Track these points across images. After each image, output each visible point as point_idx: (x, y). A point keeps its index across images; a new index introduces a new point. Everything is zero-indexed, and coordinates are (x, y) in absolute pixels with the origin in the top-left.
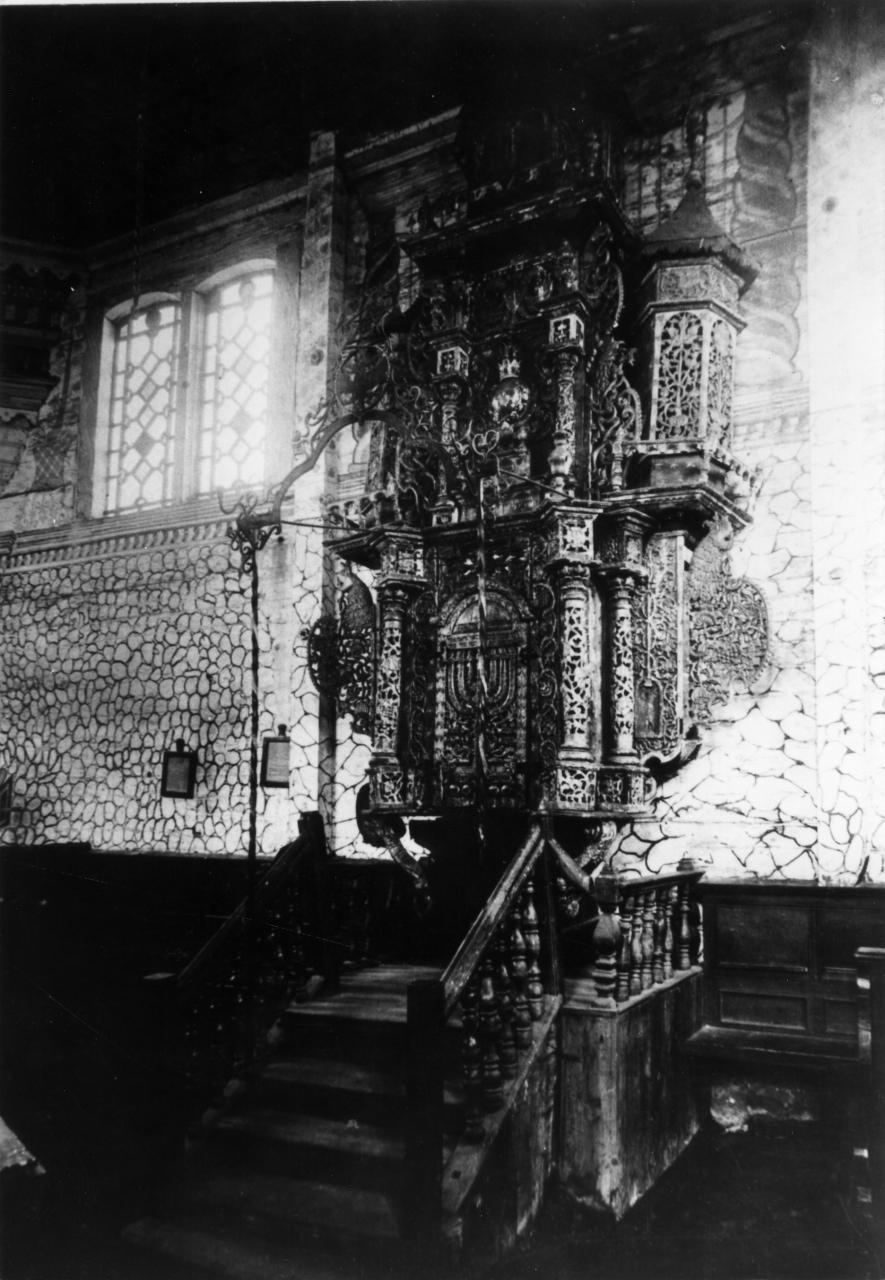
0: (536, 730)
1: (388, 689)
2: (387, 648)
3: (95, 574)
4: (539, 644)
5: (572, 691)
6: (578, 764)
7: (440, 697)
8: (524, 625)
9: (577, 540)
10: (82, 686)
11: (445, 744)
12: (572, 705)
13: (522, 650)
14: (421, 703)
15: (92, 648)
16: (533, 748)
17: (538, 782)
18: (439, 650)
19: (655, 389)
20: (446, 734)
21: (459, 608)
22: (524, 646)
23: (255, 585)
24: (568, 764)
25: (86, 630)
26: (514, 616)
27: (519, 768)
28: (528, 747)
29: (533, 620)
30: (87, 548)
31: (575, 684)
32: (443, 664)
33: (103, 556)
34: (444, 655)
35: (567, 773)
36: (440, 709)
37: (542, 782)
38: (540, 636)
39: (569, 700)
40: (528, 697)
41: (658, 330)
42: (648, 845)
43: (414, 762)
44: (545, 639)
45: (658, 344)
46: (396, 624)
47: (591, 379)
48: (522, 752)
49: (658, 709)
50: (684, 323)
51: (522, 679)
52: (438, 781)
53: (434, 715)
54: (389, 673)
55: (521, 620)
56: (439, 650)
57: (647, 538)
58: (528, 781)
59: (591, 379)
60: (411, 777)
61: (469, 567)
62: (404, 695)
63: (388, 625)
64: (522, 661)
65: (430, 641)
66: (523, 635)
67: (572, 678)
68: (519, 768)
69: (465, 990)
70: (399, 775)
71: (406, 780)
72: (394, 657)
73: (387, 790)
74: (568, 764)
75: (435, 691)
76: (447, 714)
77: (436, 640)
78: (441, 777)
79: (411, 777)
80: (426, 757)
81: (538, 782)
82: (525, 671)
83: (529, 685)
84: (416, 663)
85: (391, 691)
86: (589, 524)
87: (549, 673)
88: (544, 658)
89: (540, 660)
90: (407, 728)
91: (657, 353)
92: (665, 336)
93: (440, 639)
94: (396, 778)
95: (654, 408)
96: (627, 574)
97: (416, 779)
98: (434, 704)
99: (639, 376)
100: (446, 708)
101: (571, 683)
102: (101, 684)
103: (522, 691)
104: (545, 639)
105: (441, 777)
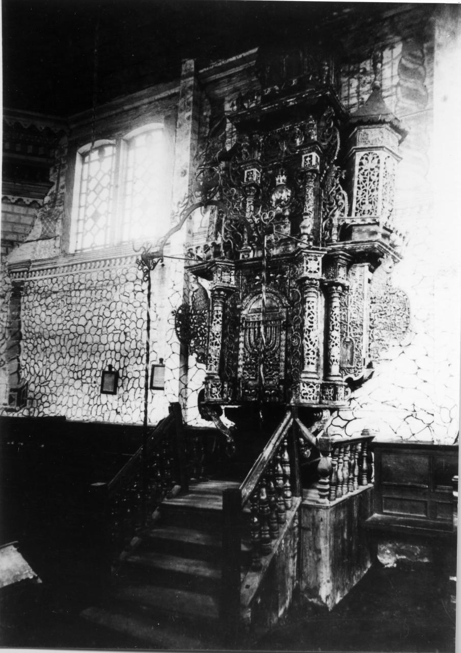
0: (290, 363)
1: (215, 341)
2: (215, 320)
3: (70, 281)
8: (285, 310)
9: (312, 268)
10: (62, 337)
11: (243, 369)
12: (308, 350)
14: (231, 348)
15: (68, 318)
16: (288, 372)
18: (241, 322)
19: (355, 190)
21: (252, 301)
22: (285, 320)
24: (306, 380)
25: (65, 309)
26: (280, 305)
27: (281, 382)
28: (285, 371)
30: (66, 268)
31: (310, 340)
32: (243, 329)
33: (74, 272)
34: (244, 324)
35: (305, 385)
36: (241, 352)
37: (292, 389)
38: (293, 316)
40: (286, 346)
41: (357, 161)
43: (227, 378)
45: (357, 168)
46: (220, 308)
47: (323, 186)
48: (282, 374)
49: (352, 353)
50: (370, 157)
51: (283, 337)
52: (240, 388)
53: (238, 355)
54: (215, 333)
55: (283, 307)
56: (241, 322)
57: (349, 266)
59: (323, 186)
60: (226, 386)
62: (223, 344)
64: (283, 328)
65: (237, 317)
66: (284, 315)
67: (309, 336)
68: (281, 382)
69: (252, 494)
70: (220, 384)
71: (223, 387)
73: (213, 392)
74: (306, 380)
75: (239, 342)
76: (245, 354)
77: (240, 317)
78: (241, 386)
79: (226, 386)
80: (233, 375)
81: (290, 389)
83: (286, 340)
84: (230, 328)
85: (216, 342)
86: (320, 259)
87: (297, 334)
88: (294, 327)
89: (293, 327)
90: (224, 361)
91: (357, 173)
92: (361, 164)
93: (242, 316)
95: (355, 201)
96: (338, 284)
97: (228, 387)
98: (238, 349)
99: (347, 184)
100: (244, 351)
101: (308, 339)
102: (72, 336)
103: (283, 343)
105: (241, 386)
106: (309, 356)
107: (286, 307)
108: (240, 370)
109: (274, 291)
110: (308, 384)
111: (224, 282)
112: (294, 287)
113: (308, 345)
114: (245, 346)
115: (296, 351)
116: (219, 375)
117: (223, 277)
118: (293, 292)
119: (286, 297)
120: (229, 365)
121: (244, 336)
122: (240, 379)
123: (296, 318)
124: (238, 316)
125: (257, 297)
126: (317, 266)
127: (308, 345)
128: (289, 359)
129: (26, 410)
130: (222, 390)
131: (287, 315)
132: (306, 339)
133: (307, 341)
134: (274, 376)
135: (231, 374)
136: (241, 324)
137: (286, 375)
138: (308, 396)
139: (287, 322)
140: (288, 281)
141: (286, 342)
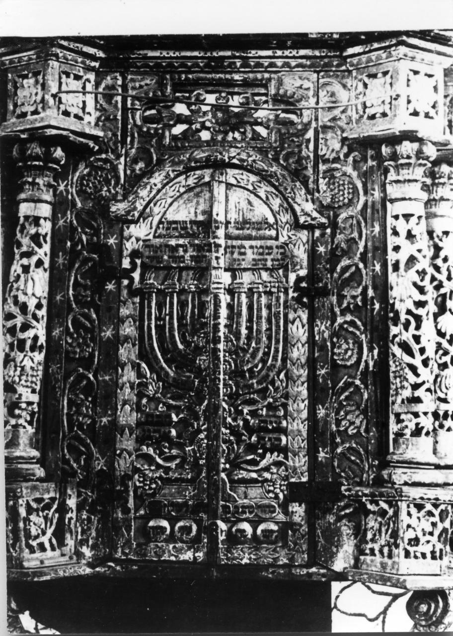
0: (326, 423)
1: (31, 333)
2: (28, 254)
4: (332, 270)
5: (417, 361)
6: (431, 493)
7: (126, 353)
8: (304, 235)
11: (140, 441)
12: (416, 387)
13: (299, 280)
14: (87, 363)
16: (322, 455)
17: (331, 519)
18: (126, 263)
20: (139, 424)
21: (171, 191)
22: (303, 273)
23: (248, 190)
24: (415, 493)
26: (285, 218)
27: (295, 493)
28: (312, 452)
29: (322, 226)
31: (422, 351)
32: (133, 293)
34: (136, 275)
35: (413, 510)
36: (129, 375)
37: (339, 519)
38: (334, 257)
39: (412, 379)
40: (312, 364)
42: (390, 598)
43: (74, 474)
44: (345, 262)
46: (45, 210)
48: (300, 462)
51: (299, 332)
52: (126, 511)
53: (116, 385)
54: (32, 303)
55: (297, 226)
56: (126, 263)
58: (311, 517)
60: (72, 503)
61: (180, 119)
62: (52, 349)
63: (25, 209)
64: (298, 300)
65: (108, 248)
66: (301, 254)
67: (417, 339)
68: (295, 493)
70: (53, 500)
71: (63, 509)
72: (40, 270)
73: (34, 531)
74: (415, 493)
75: (118, 341)
76: (143, 385)
77: (120, 245)
78: (131, 504)
79: (72, 503)
80: (100, 465)
81: (331, 519)
82: (305, 317)
83: (311, 341)
84: (76, 284)
85: (36, 338)
87: (352, 323)
88: (341, 298)
89: (334, 299)
90: (58, 412)
93: (129, 246)
94: (48, 507)
97: (80, 507)
98: (112, 363)
100: (140, 375)
101: (415, 347)
103: (299, 353)
104: (345, 262)
105: (131, 504)
106: (419, 408)
107: (310, 228)
108: (127, 443)
109: (261, 165)
110: (420, 507)
111: (66, 113)
112: (336, 160)
113: (413, 369)
114: (145, 354)
115: (348, 385)
116: (42, 462)
117: (64, 97)
118: (330, 174)
119: (309, 192)
120: (80, 426)
121: (140, 319)
122: (128, 477)
123: (346, 269)
124: (112, 241)
125: (191, 181)
126: (433, 97)
127: (413, 369)
128: (321, 412)
129: (231, 103)
130: (61, 520)
131: (313, 255)
132: (406, 348)
133: (410, 353)
134: (267, 469)
135: (90, 457)
136: (127, 274)
137: (314, 465)
138: (421, 549)
139: (312, 277)
140: (310, 134)
141: (311, 351)
